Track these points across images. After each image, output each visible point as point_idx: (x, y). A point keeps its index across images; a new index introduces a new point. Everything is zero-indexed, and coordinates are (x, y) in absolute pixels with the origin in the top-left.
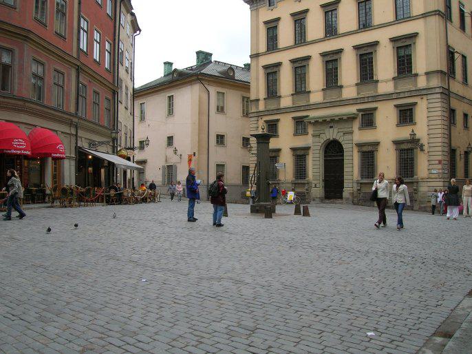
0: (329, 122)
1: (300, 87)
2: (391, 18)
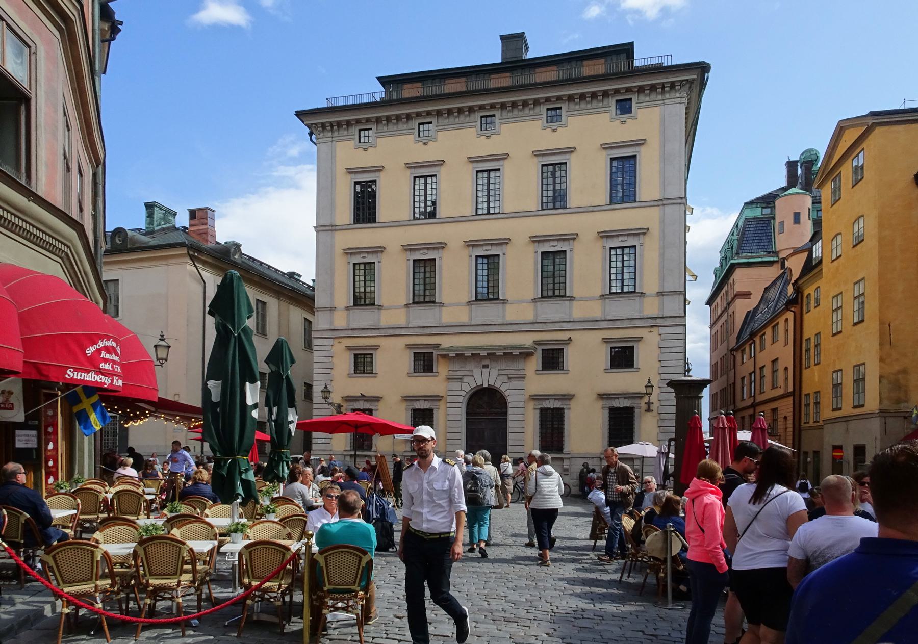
0: (484, 358)
1: (424, 292)
2: (469, 210)
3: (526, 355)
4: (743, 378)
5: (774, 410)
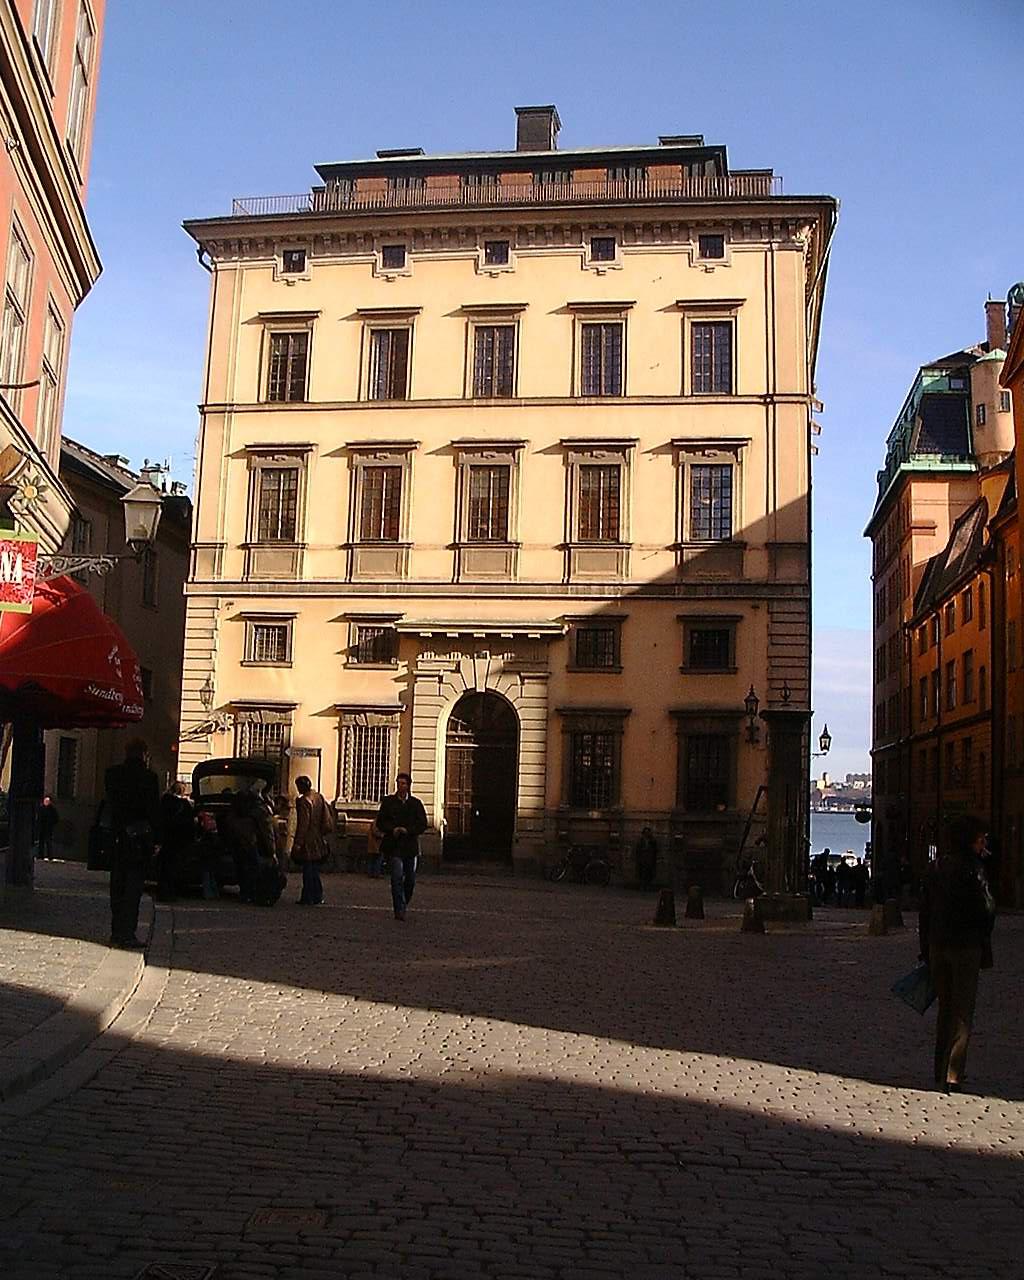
4: (950, 664)
5: (967, 742)
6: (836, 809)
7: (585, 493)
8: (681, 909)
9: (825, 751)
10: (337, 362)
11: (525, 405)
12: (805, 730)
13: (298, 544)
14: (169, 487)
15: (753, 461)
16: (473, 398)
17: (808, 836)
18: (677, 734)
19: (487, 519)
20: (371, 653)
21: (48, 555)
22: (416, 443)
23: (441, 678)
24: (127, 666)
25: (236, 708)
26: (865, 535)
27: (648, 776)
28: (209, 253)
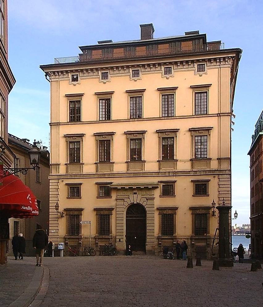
3: (155, 188)
6: (239, 235)
7: (163, 146)
8: (194, 263)
9: (236, 218)
10: (90, 109)
11: (146, 120)
12: (230, 212)
13: (81, 163)
14: (42, 148)
15: (214, 134)
16: (130, 119)
17: (231, 242)
18: (192, 214)
19: (136, 155)
20: (104, 194)
21: (7, 168)
22: (114, 133)
23: (124, 200)
24: (33, 200)
25: (66, 210)
26: (248, 154)
27: (184, 227)
28: (49, 76)
